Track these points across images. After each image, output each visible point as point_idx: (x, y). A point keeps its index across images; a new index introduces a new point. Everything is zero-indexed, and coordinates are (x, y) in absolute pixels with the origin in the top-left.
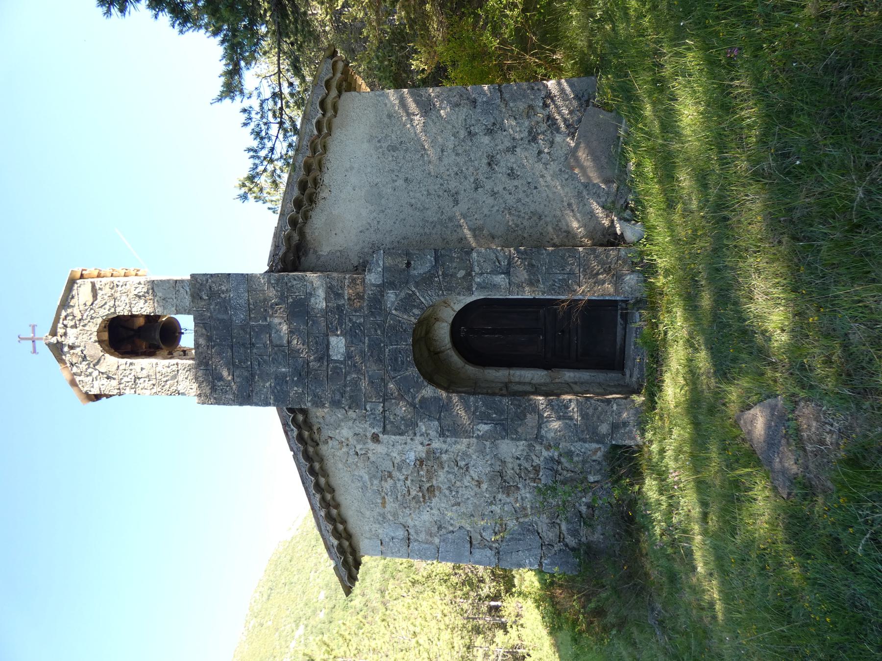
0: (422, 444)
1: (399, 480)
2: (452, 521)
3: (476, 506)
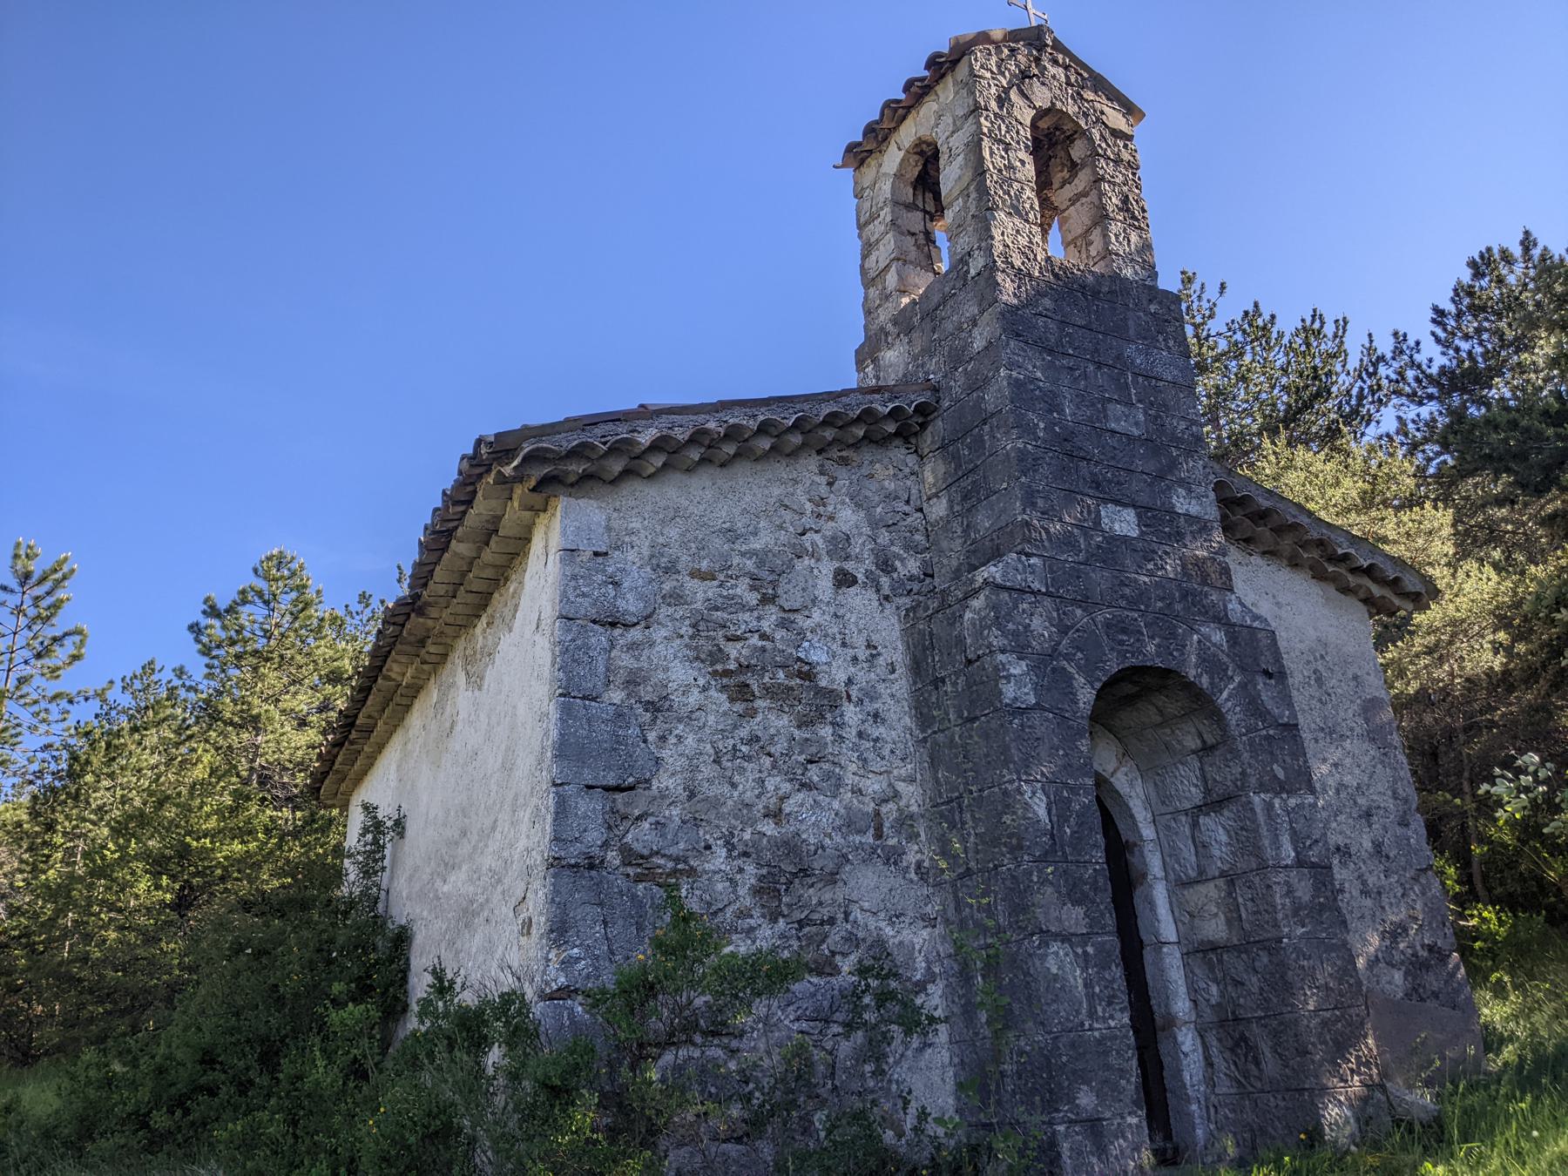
0: (850, 682)
1: (759, 619)
2: (673, 740)
3: (716, 803)
